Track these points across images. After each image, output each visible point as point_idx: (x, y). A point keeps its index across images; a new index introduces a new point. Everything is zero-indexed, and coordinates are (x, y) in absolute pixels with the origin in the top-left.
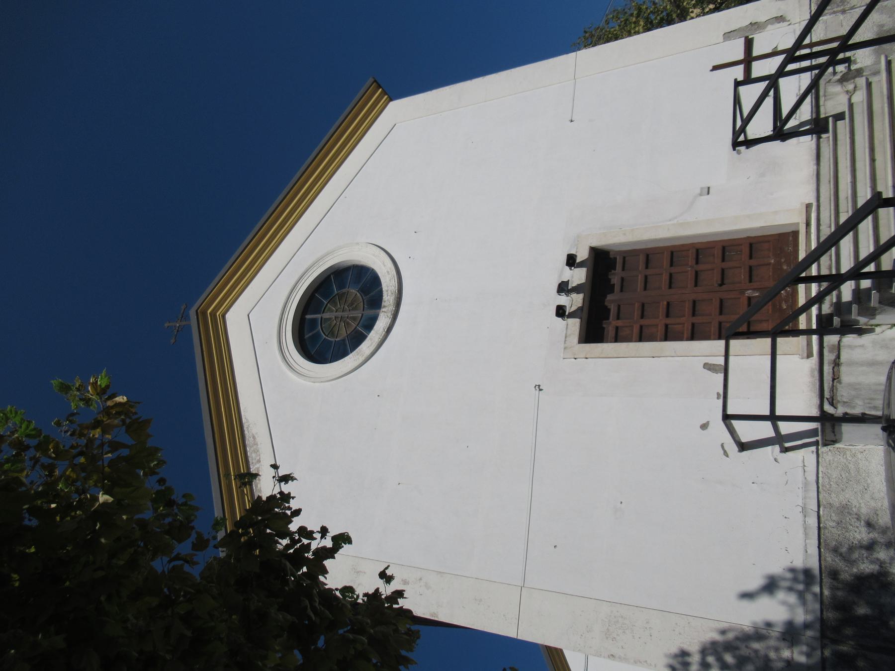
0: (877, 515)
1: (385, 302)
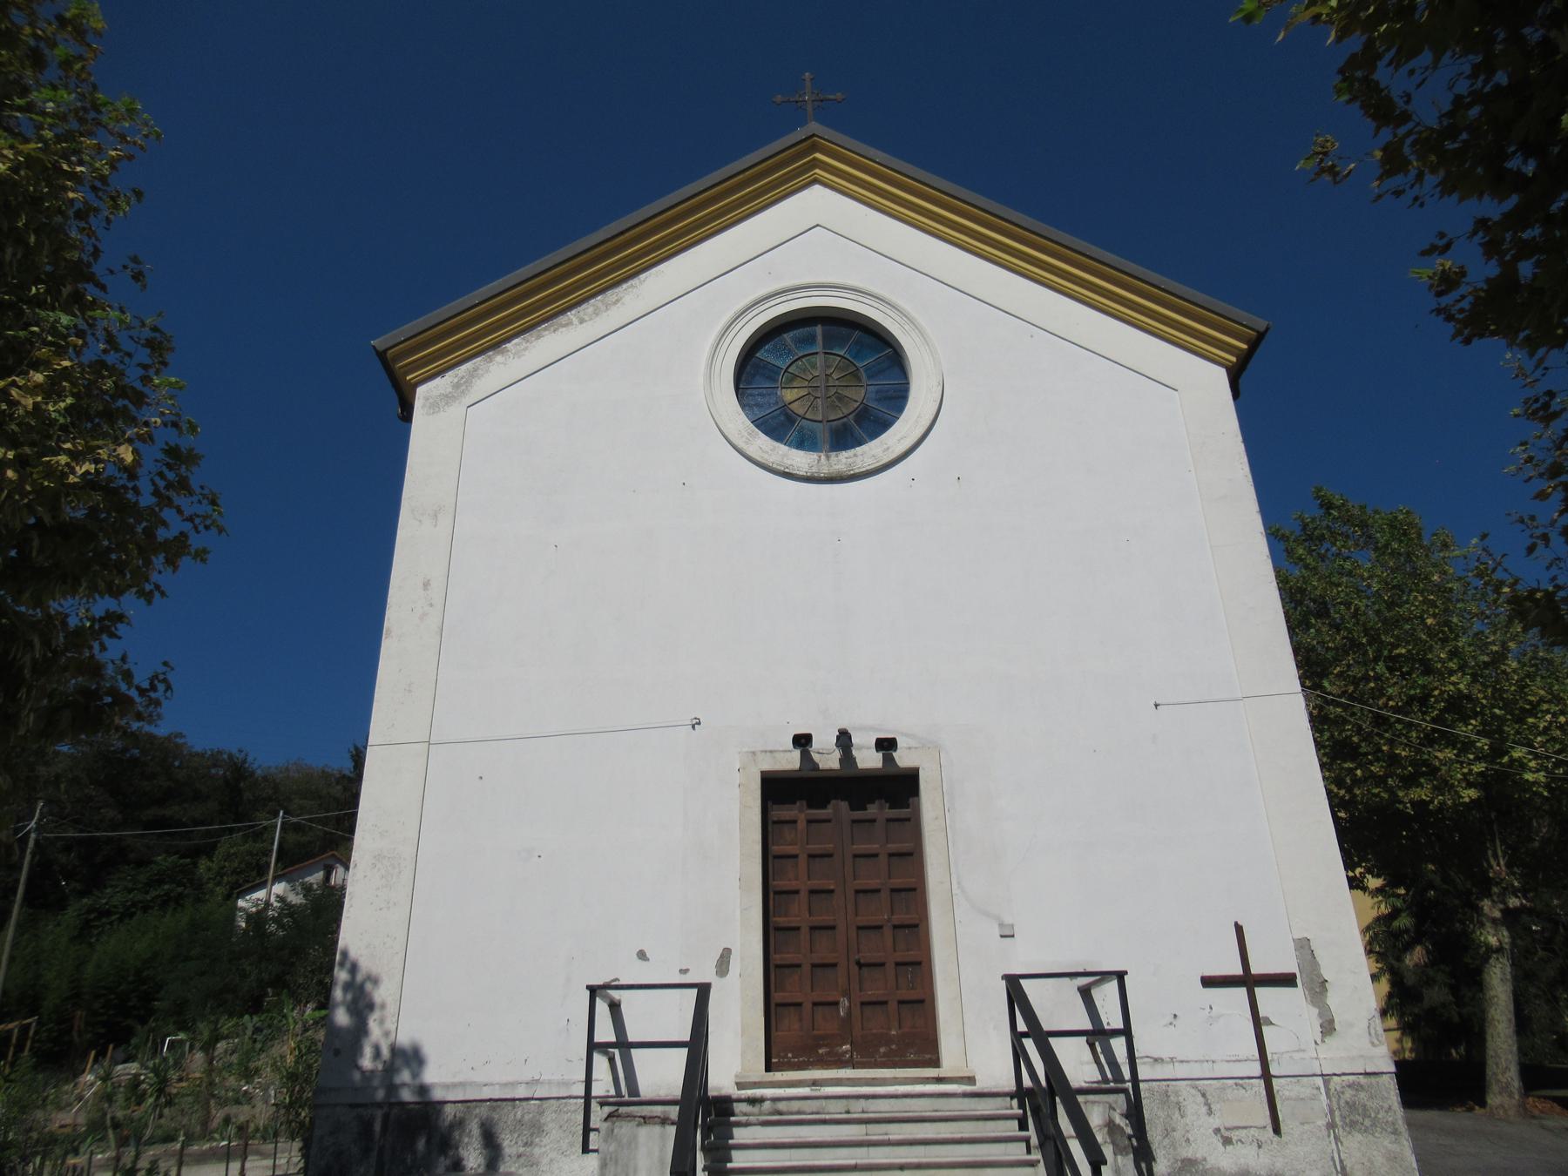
0: (532, 1166)
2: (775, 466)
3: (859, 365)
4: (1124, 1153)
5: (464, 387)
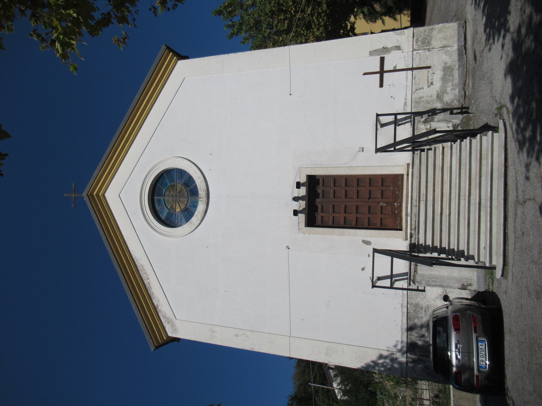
1: (200, 195)
2: (202, 216)
3: (169, 185)
4: (434, 118)
5: (169, 320)
